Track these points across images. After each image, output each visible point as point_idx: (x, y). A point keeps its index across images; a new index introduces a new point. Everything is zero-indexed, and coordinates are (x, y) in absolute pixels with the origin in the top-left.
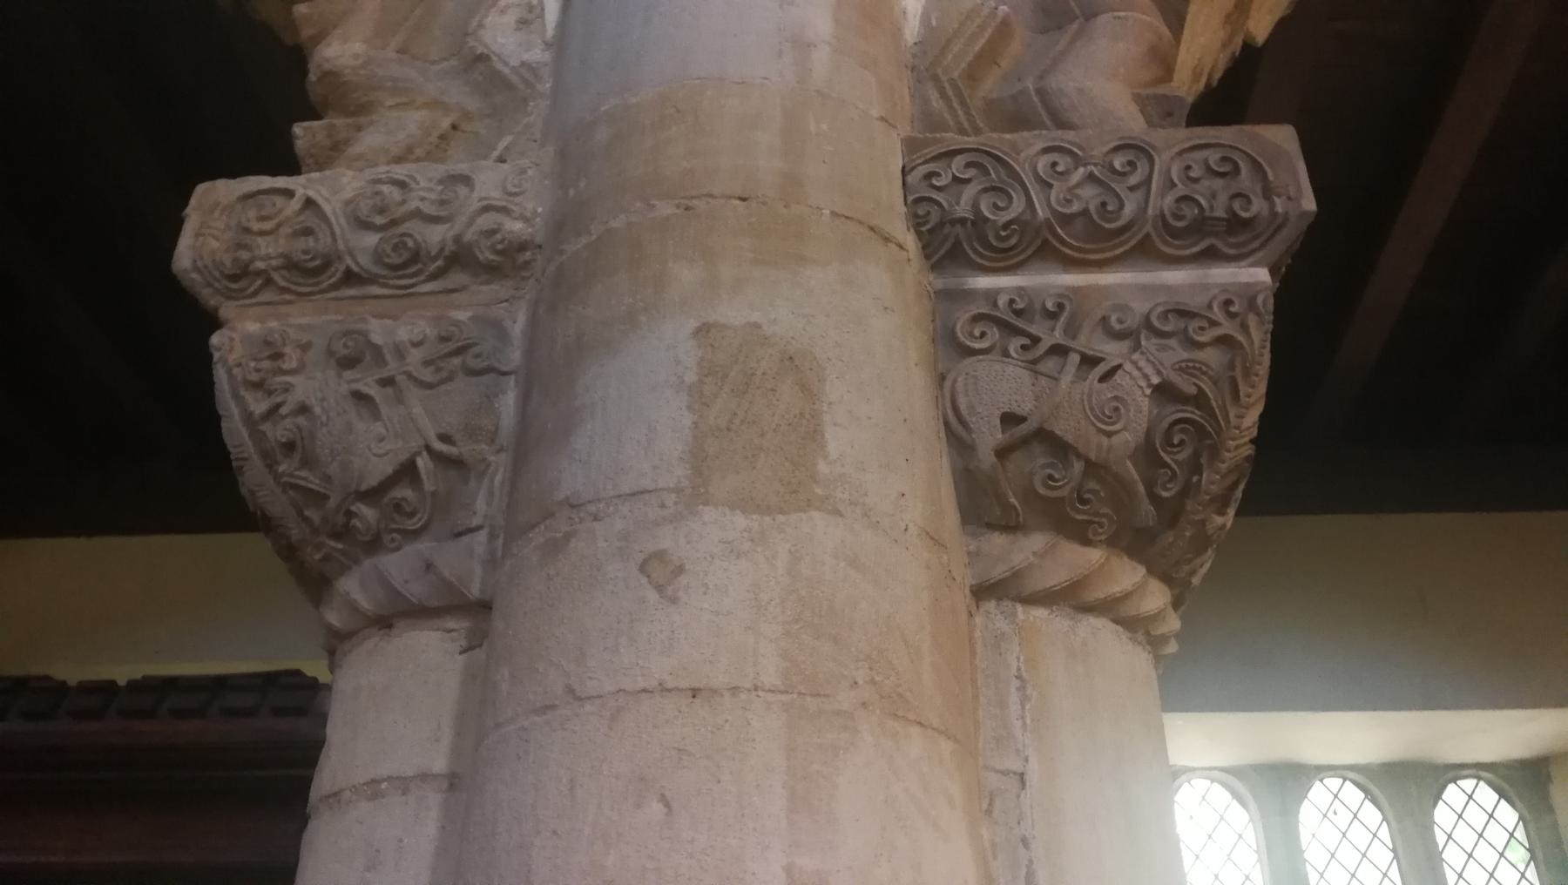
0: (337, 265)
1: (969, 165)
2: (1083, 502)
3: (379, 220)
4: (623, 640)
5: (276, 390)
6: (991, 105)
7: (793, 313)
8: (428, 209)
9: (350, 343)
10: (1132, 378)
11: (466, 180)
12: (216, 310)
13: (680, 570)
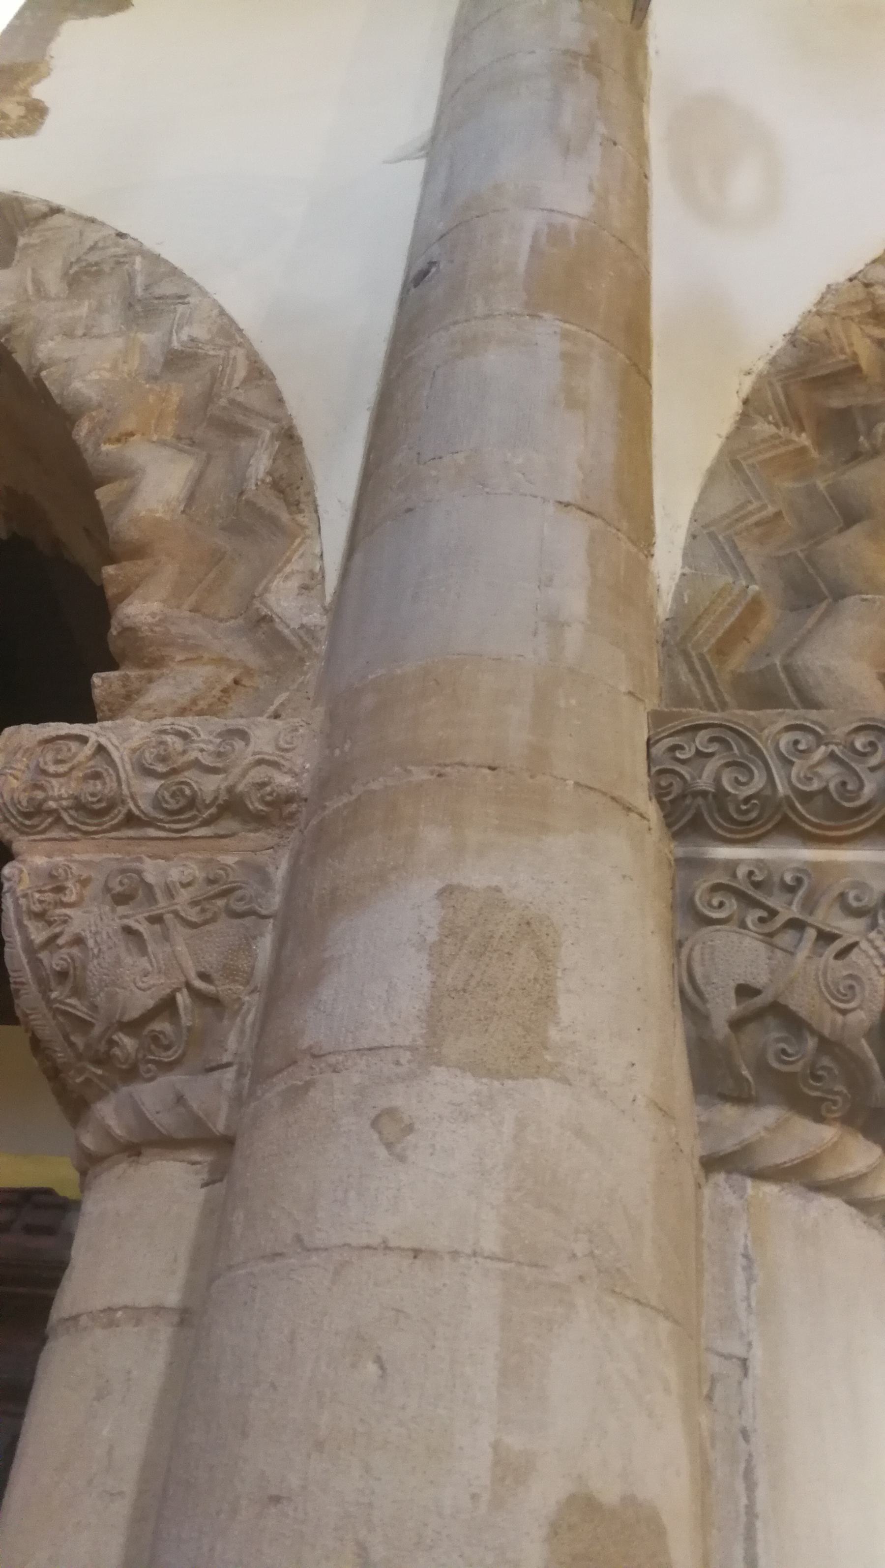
0: (120, 808)
1: (712, 740)
2: (818, 1078)
3: (161, 768)
4: (352, 1194)
5: (55, 921)
6: (739, 681)
7: (533, 879)
8: (207, 760)
9: (126, 881)
10: (868, 956)
11: (243, 735)
12: (10, 842)
13: (410, 1129)
